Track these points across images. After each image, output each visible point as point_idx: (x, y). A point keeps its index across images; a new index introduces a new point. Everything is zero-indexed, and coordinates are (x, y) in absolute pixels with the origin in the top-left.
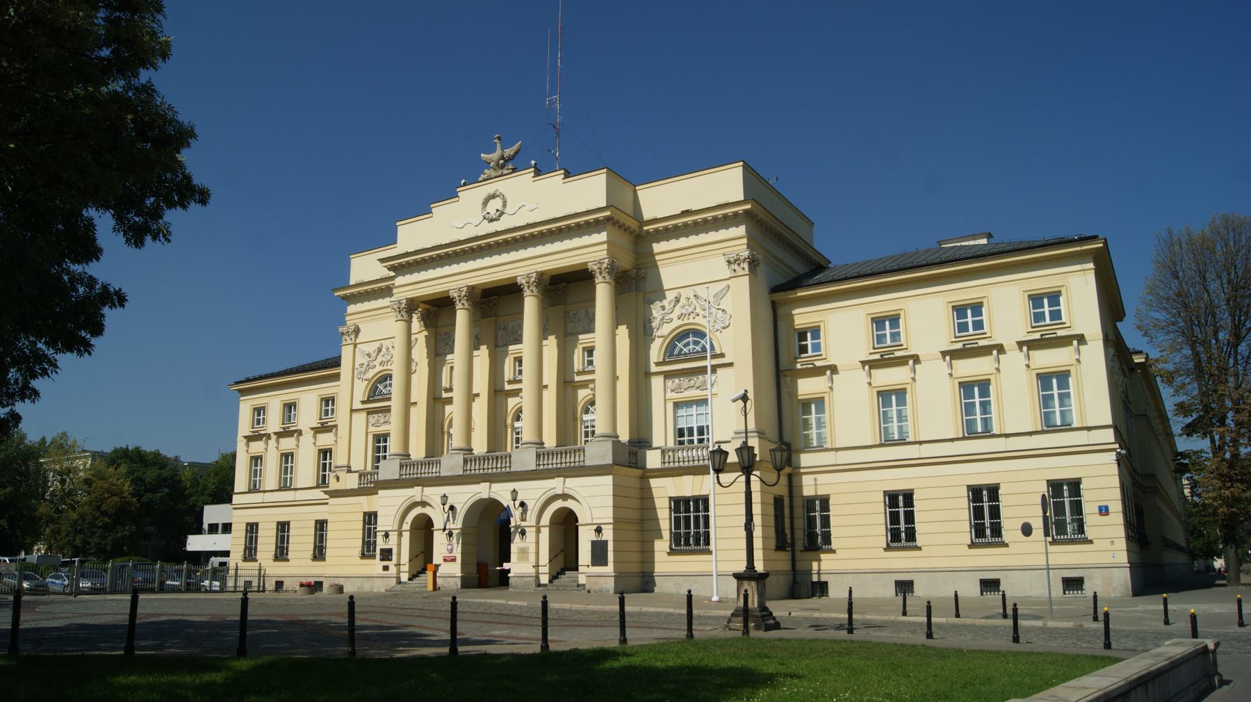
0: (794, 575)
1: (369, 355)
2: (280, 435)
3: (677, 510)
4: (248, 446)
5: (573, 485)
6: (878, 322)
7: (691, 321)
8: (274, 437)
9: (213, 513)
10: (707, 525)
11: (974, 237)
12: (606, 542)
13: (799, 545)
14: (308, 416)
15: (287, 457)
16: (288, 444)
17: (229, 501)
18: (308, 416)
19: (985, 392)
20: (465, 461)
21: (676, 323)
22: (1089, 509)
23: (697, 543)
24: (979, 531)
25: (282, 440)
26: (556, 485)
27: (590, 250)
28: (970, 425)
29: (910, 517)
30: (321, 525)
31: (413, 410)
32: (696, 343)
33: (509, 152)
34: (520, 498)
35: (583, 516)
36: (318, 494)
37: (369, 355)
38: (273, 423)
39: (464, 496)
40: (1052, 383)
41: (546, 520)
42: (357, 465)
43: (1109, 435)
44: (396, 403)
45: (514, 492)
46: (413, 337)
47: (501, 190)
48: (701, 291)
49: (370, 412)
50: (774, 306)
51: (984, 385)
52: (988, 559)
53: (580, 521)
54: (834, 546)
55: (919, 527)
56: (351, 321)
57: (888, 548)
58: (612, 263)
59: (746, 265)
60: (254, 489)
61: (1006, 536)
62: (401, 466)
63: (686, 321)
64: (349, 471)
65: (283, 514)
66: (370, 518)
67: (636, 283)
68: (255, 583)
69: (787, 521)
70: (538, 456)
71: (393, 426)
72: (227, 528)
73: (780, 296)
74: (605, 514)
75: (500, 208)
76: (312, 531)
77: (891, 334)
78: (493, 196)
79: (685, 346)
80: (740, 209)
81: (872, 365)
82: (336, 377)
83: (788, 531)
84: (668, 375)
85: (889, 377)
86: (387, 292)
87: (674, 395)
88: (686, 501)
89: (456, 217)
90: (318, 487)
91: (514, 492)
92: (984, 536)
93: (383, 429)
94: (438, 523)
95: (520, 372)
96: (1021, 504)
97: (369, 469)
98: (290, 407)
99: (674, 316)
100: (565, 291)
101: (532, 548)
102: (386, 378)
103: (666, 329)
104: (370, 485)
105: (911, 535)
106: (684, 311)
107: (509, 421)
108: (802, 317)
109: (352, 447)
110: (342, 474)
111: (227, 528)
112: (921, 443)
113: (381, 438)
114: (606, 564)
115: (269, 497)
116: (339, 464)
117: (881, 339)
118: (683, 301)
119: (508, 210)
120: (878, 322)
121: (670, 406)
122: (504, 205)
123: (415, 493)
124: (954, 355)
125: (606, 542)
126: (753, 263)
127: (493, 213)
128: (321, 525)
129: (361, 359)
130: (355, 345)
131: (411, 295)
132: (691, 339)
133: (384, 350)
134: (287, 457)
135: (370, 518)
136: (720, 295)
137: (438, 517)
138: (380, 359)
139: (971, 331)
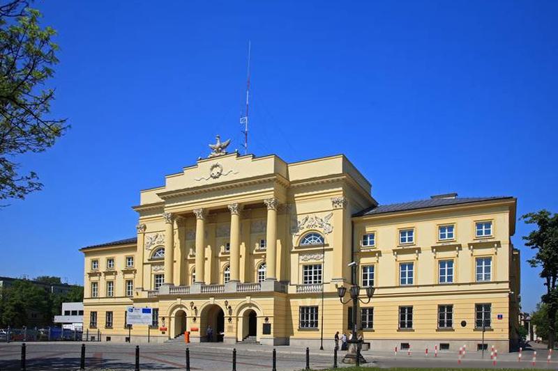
1: (151, 238)
3: (303, 312)
5: (255, 300)
6: (442, 229)
7: (313, 228)
8: (103, 274)
11: (449, 195)
12: (270, 324)
15: (110, 283)
22: (493, 316)
23: (312, 326)
24: (441, 324)
27: (266, 195)
32: (315, 239)
33: (224, 144)
38: (102, 267)
39: (201, 304)
40: (446, 268)
41: (241, 314)
42: (147, 287)
43: (507, 286)
47: (219, 163)
49: (153, 265)
51: (488, 260)
52: (445, 336)
53: (258, 316)
56: (141, 223)
59: (341, 204)
61: (454, 326)
62: (170, 289)
64: (143, 290)
67: (286, 210)
68: (96, 337)
73: (356, 219)
74: (271, 313)
76: (105, 316)
78: (216, 166)
79: (310, 240)
84: (300, 253)
85: (129, 276)
86: (161, 210)
87: (303, 262)
88: (307, 308)
89: (197, 176)
92: (405, 327)
93: (160, 272)
96: (464, 311)
97: (153, 289)
98: (111, 260)
101: (235, 326)
102: (161, 250)
103: (301, 232)
105: (410, 325)
107: (256, 269)
108: (369, 229)
109: (144, 279)
114: (269, 333)
115: (102, 301)
118: (159, 236)
119: (223, 173)
120: (403, 233)
121: (153, 276)
125: (270, 324)
127: (216, 174)
130: (144, 234)
131: (240, 201)
132: (313, 237)
134: (110, 283)
137: (190, 313)
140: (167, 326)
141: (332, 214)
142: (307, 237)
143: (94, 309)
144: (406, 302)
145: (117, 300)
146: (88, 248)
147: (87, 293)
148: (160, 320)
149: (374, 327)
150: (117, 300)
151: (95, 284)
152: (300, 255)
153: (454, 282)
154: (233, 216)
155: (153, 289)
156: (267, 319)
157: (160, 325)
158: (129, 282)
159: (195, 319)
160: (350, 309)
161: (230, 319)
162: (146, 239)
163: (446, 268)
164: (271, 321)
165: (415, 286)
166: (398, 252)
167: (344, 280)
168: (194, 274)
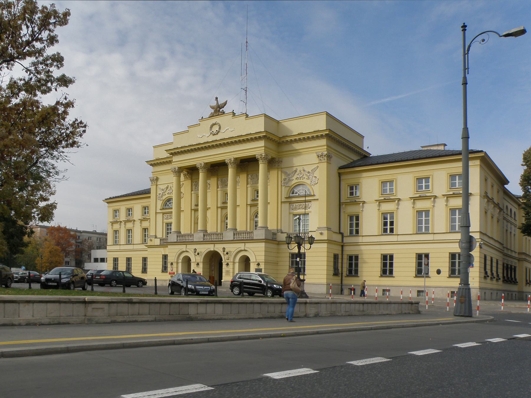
0: (342, 286)
2: (126, 222)
4: (379, 205)
5: (249, 245)
6: (384, 183)
8: (123, 223)
9: (97, 253)
10: (304, 264)
13: (344, 274)
14: (137, 214)
15: (129, 231)
16: (129, 225)
17: (106, 248)
18: (137, 214)
19: (427, 215)
20: (204, 235)
21: (167, 196)
25: (143, 222)
26: (241, 246)
27: (257, 149)
28: (420, 229)
29: (391, 265)
30: (145, 260)
31: (269, 206)
34: (226, 250)
35: (252, 259)
36: (143, 247)
37: (163, 190)
39: (205, 249)
40: (422, 218)
41: (237, 259)
42: (159, 235)
44: (174, 210)
45: (224, 249)
46: (181, 183)
48: (306, 168)
50: (340, 175)
51: (427, 212)
52: (420, 282)
54: (359, 275)
55: (394, 269)
57: (450, 277)
58: (266, 155)
59: (326, 158)
60: (116, 243)
61: (430, 274)
62: (177, 236)
63: (299, 181)
65: (129, 254)
66: (165, 257)
69: (340, 265)
70: (234, 234)
71: (173, 220)
72: (103, 260)
73: (342, 171)
74: (261, 258)
75: (217, 129)
76: (447, 260)
77: (390, 189)
80: (324, 133)
81: (380, 202)
82: (150, 197)
83: (340, 269)
85: (422, 205)
86: (170, 162)
90: (143, 244)
91: (224, 249)
92: (352, 274)
93: (169, 221)
94: (193, 260)
95: (258, 196)
96: (440, 261)
97: (164, 237)
98: (129, 210)
99: (166, 193)
100: (246, 164)
101: (231, 271)
102: (169, 200)
104: (164, 243)
105: (391, 272)
106: (298, 176)
109: (157, 228)
110: (153, 239)
111: (103, 260)
112: (398, 235)
113: (169, 225)
116: (151, 235)
117: (420, 187)
120: (384, 183)
121: (164, 224)
122: (220, 128)
123: (183, 247)
124: (415, 199)
126: (329, 157)
128: (145, 260)
129: (159, 192)
130: (157, 185)
133: (169, 188)
134: (129, 231)
135: (165, 257)
136: (314, 170)
138: (167, 192)
139: (424, 189)
140: (175, 270)
141: (318, 166)
142: (168, 202)
143: (116, 255)
144: (422, 249)
145: (437, 237)
146: (110, 198)
147: (110, 241)
148: (169, 265)
149: (394, 273)
150: (437, 237)
151: (116, 232)
152: (290, 203)
153: (395, 233)
154: (229, 169)
155: (164, 237)
156: (258, 264)
157: (169, 270)
158: (145, 230)
159: (198, 264)
160: (336, 257)
161: (228, 264)
162: (158, 190)
163: (422, 218)
164: (262, 266)
165: (396, 235)
166: (415, 199)
167: (329, 229)
168: (145, 224)
